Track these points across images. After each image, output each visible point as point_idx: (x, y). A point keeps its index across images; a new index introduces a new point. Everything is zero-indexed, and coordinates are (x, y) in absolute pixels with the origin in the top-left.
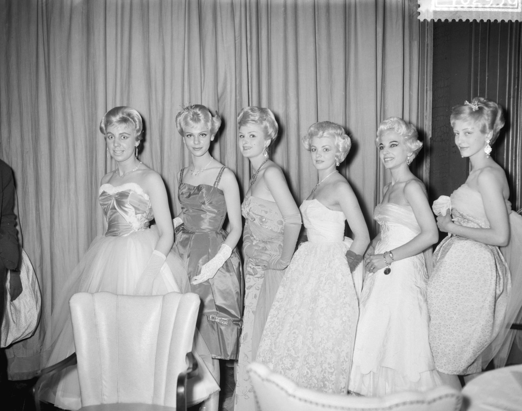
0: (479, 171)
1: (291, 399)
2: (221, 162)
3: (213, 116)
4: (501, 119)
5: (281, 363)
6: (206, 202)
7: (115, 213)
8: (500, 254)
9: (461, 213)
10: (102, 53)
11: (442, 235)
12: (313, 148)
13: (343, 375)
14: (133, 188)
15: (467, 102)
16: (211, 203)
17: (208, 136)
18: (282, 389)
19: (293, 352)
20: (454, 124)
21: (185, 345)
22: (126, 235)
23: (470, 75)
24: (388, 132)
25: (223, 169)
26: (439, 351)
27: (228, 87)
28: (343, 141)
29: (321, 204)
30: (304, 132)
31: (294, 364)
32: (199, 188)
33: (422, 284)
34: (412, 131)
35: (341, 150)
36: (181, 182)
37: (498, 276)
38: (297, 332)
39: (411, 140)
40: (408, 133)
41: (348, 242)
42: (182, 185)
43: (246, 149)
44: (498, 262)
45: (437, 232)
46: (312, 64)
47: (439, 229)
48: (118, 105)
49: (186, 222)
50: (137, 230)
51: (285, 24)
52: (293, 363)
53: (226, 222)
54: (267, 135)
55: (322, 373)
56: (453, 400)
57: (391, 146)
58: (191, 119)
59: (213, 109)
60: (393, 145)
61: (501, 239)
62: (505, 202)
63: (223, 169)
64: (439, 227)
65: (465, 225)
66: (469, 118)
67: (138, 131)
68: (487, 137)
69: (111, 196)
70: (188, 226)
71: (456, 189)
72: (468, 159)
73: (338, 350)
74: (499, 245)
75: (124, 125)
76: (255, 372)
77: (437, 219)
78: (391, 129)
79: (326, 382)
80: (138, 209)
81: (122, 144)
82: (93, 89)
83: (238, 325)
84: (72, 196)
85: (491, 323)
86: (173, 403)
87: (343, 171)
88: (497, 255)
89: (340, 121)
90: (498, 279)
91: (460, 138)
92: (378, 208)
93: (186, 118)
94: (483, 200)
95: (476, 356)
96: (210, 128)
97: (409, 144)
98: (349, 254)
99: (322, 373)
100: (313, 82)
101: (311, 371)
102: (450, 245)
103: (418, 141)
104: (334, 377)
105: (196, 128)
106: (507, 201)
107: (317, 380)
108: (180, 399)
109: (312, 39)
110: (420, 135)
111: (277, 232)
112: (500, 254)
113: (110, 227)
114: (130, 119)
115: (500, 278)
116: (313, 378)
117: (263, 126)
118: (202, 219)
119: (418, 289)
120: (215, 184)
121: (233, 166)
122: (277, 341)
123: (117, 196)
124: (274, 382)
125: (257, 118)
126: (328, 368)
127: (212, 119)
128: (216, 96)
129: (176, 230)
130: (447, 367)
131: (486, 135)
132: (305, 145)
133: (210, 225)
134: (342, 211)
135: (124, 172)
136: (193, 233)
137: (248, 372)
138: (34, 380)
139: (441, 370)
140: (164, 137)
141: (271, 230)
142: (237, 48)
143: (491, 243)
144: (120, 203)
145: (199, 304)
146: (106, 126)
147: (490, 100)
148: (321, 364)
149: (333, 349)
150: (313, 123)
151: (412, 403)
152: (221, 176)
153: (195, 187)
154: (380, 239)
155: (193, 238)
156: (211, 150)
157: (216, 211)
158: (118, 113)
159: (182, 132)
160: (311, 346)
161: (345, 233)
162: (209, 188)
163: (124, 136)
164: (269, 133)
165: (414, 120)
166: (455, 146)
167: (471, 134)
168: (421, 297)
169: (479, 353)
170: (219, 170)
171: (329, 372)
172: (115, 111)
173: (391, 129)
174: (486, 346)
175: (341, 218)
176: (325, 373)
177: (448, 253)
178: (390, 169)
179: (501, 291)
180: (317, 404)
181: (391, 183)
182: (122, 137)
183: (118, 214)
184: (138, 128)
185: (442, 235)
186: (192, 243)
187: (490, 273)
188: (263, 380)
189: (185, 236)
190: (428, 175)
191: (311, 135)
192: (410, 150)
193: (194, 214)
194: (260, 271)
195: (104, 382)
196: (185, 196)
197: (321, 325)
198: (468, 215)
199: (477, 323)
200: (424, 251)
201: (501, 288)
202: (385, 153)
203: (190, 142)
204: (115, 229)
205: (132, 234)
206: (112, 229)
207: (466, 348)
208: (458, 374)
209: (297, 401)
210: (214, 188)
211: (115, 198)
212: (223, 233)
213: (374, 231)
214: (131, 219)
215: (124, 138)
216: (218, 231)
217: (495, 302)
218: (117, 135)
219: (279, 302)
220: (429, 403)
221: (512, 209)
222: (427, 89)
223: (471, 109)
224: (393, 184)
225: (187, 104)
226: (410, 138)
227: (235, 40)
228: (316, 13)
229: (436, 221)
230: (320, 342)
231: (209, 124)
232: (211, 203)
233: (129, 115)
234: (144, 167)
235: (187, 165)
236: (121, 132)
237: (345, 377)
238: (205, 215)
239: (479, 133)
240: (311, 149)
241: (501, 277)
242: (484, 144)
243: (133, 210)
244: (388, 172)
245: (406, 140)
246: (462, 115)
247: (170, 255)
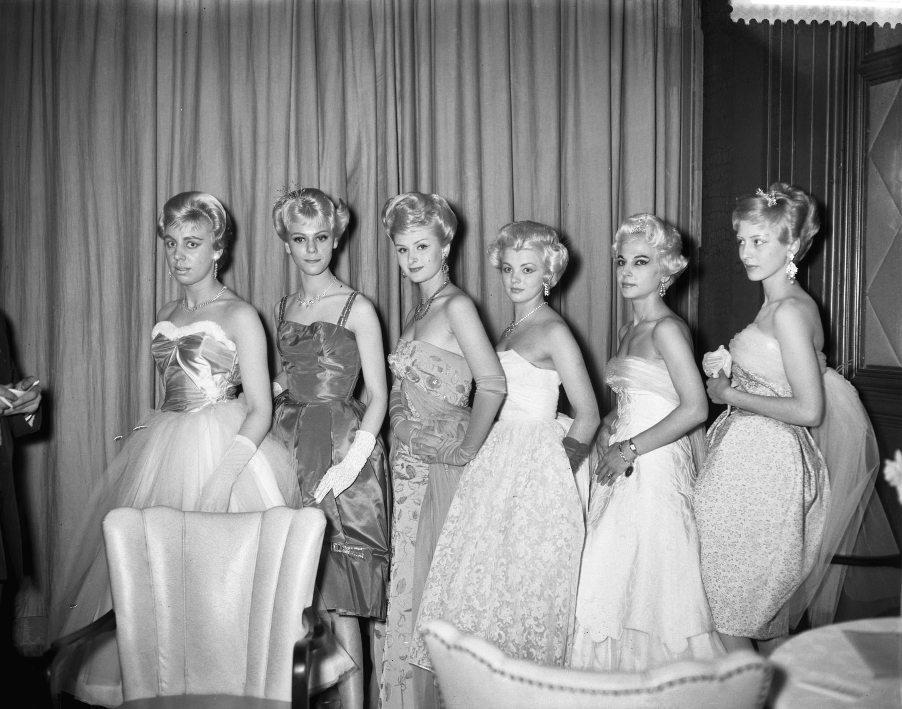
0: (776, 304)
1: (497, 676)
2: (351, 287)
3: (336, 207)
4: (815, 220)
5: (457, 621)
6: (325, 352)
7: (177, 371)
8: (810, 437)
9: (746, 370)
10: (150, 100)
11: (715, 410)
12: (506, 266)
13: (558, 636)
14: (209, 329)
15: (760, 192)
16: (332, 354)
17: (330, 239)
18: (482, 661)
19: (476, 603)
20: (738, 226)
21: (300, 595)
22: (196, 410)
23: (765, 146)
24: (634, 238)
25: (353, 298)
26: (718, 599)
27: (364, 160)
28: (555, 254)
29: (521, 358)
30: (491, 237)
31: (479, 623)
32: (313, 328)
33: (686, 489)
34: (674, 240)
35: (552, 269)
36: (282, 320)
37: (806, 471)
38: (482, 568)
39: (670, 257)
40: (667, 242)
41: (565, 422)
42: (283, 325)
44: (805, 450)
45: (706, 404)
46: (504, 124)
47: (709, 400)
49: (291, 388)
50: (214, 402)
51: (460, 56)
52: (476, 621)
53: (360, 383)
55: (525, 635)
56: (759, 674)
57: (636, 264)
58: (301, 211)
59: (336, 197)
60: (641, 261)
61: (809, 414)
62: (816, 355)
63: (353, 298)
64: (711, 396)
65: (751, 390)
66: (761, 218)
68: (790, 250)
69: (171, 343)
70: (295, 395)
71: (740, 331)
72: (760, 284)
73: (550, 596)
74: (809, 425)
76: (436, 636)
77: (708, 383)
78: (638, 233)
79: (532, 650)
80: (217, 366)
81: (188, 255)
82: (133, 161)
83: (384, 559)
84: (95, 343)
85: (799, 549)
86: (284, 693)
87: (556, 303)
88: (805, 440)
89: (549, 218)
90: (806, 476)
91: (746, 250)
92: (613, 365)
93: (291, 209)
94: (781, 351)
95: (780, 606)
96: (332, 226)
98: (568, 442)
99: (525, 635)
100: (506, 153)
101: (506, 633)
102: (727, 424)
103: (682, 257)
104: (545, 640)
105: (310, 227)
106: (819, 352)
107: (517, 646)
108: (298, 683)
109: (503, 81)
110: (686, 247)
111: (453, 405)
112: (810, 437)
113: (169, 394)
115: (810, 476)
116: (510, 644)
117: (433, 224)
118: (319, 381)
119: (683, 499)
120: (339, 322)
121: (371, 292)
122: (452, 586)
123: (181, 343)
124: (468, 651)
126: (534, 626)
127: (335, 212)
128: (343, 173)
129: (275, 402)
130: (731, 624)
131: (789, 246)
132: (494, 261)
133: (332, 391)
134: (554, 369)
135: (196, 303)
136: (303, 405)
137: (422, 635)
138: (52, 654)
139: (721, 630)
140: (261, 248)
141: (446, 401)
142: (379, 95)
143: (794, 422)
144: (187, 356)
145: (324, 527)
147: (797, 187)
148: (523, 619)
149: (542, 594)
150: (506, 223)
151: (694, 679)
152: (350, 308)
153: (305, 327)
154: (617, 417)
155: (303, 414)
156: (333, 266)
157: (342, 367)
159: (285, 235)
160: (504, 591)
161: (559, 407)
162: (329, 327)
163: (192, 243)
165: (673, 218)
166: (740, 263)
167: (766, 245)
168: (687, 512)
169: (784, 600)
170: (347, 298)
171: (536, 633)
172: (175, 202)
173: (638, 233)
174: (794, 589)
175: (552, 379)
176: (529, 634)
177: (725, 437)
178: (632, 299)
179: (813, 495)
180: (540, 685)
181: (633, 322)
182: (190, 245)
183: (183, 373)
184: (218, 227)
185: (715, 410)
186: (301, 423)
187: (793, 467)
188: (449, 647)
189: (290, 410)
190: (695, 310)
191: (503, 245)
192: (666, 271)
193: (304, 372)
194: (422, 470)
195: (162, 660)
196: (289, 342)
197: (521, 556)
198: (756, 375)
199: (776, 549)
200: (689, 433)
201: (813, 492)
202: (625, 273)
203: (301, 250)
204: (179, 399)
205: (206, 408)
206: (173, 399)
207: (760, 592)
208: (750, 635)
209: (506, 680)
210: (339, 327)
211: (179, 346)
212: (355, 403)
213: (606, 403)
214: (205, 382)
215: (193, 245)
216: (346, 400)
217: (804, 515)
218: (180, 241)
219: (453, 522)
220: (722, 679)
221: (828, 366)
222: (693, 167)
224: (636, 323)
225: (293, 188)
226: (668, 253)
227: (376, 82)
228: (511, 38)
229: (706, 387)
230: (521, 583)
231: (331, 219)
232: (332, 354)
233: (203, 206)
234: (229, 295)
235: (293, 290)
236: (187, 235)
237: (561, 639)
238: (322, 374)
239: (778, 243)
240: (503, 268)
241: (812, 474)
242: (785, 261)
243: (209, 366)
244: (630, 304)
245: (662, 256)
246: (751, 213)
247: (267, 442)
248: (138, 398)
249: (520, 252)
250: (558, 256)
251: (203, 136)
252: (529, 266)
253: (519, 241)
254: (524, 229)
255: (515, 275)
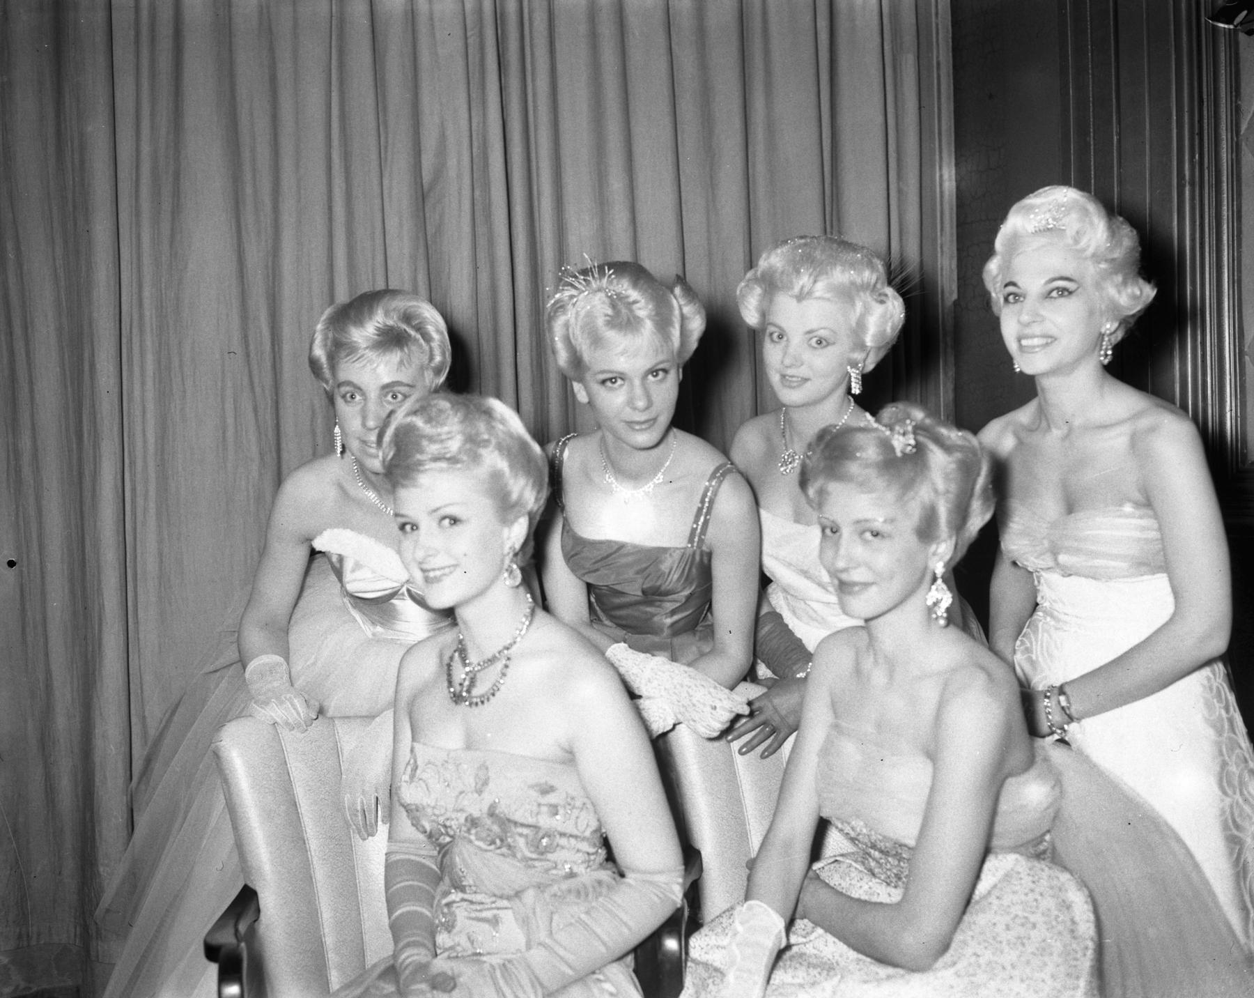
28: (878, 310)
39: (1119, 278)
40: (1111, 249)
43: (438, 580)
48: (365, 288)
54: (506, 507)
57: (1048, 296)
60: (1061, 289)
66: (880, 483)
67: (438, 371)
75: (395, 356)
84: (27, 471)
97: (1112, 291)
114: (412, 333)
117: (482, 471)
125: (454, 445)
146: (332, 358)
158: (371, 313)
164: (514, 496)
192: (1114, 307)
223: (886, 446)
233: (407, 318)
236: (386, 380)
245: (1105, 276)
248: (98, 561)
249: (804, 303)
250: (883, 316)
251: (189, 121)
252: (822, 333)
253: (804, 280)
254: (818, 254)
255: (791, 350)
